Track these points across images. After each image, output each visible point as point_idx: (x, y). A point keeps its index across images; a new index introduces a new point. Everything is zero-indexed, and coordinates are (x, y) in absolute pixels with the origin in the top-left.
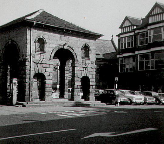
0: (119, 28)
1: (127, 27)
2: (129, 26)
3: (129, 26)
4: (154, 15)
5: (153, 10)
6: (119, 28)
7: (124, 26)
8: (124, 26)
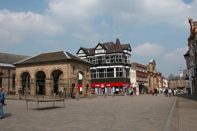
0: (77, 54)
1: (81, 53)
2: (83, 53)
3: (83, 53)
4: (80, 54)
5: (79, 51)
6: (77, 54)
7: (79, 53)
8: (79, 53)
